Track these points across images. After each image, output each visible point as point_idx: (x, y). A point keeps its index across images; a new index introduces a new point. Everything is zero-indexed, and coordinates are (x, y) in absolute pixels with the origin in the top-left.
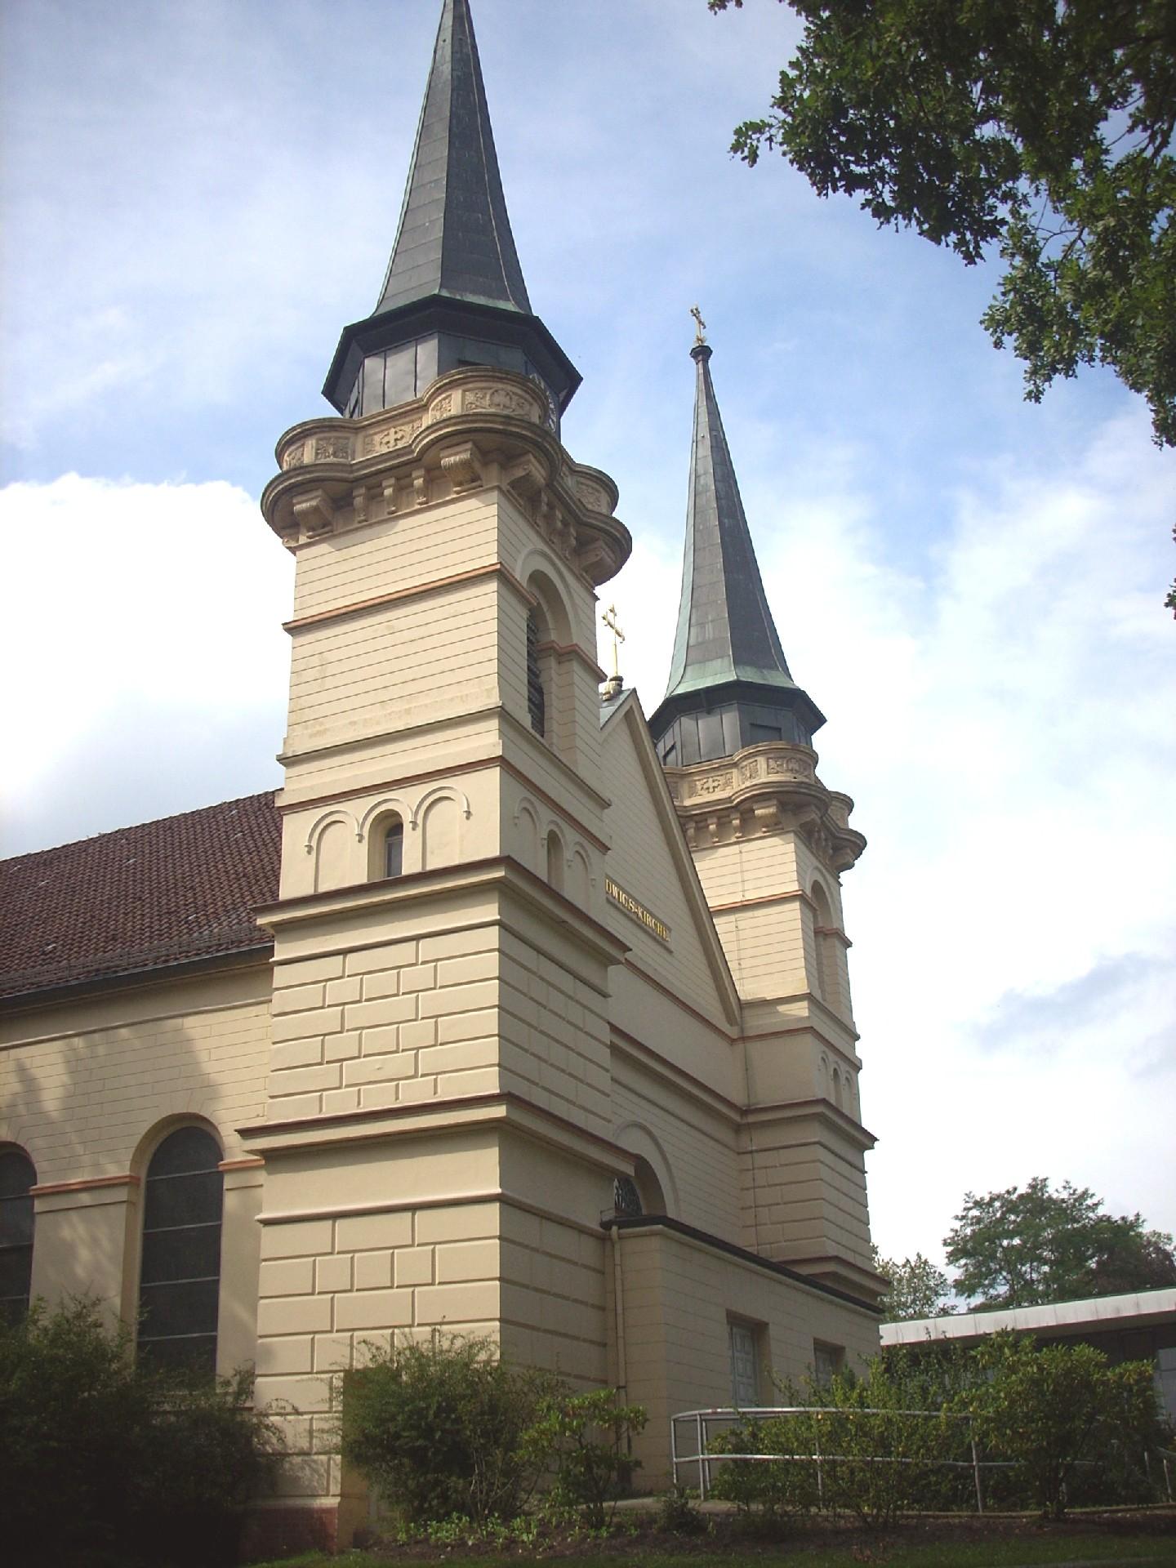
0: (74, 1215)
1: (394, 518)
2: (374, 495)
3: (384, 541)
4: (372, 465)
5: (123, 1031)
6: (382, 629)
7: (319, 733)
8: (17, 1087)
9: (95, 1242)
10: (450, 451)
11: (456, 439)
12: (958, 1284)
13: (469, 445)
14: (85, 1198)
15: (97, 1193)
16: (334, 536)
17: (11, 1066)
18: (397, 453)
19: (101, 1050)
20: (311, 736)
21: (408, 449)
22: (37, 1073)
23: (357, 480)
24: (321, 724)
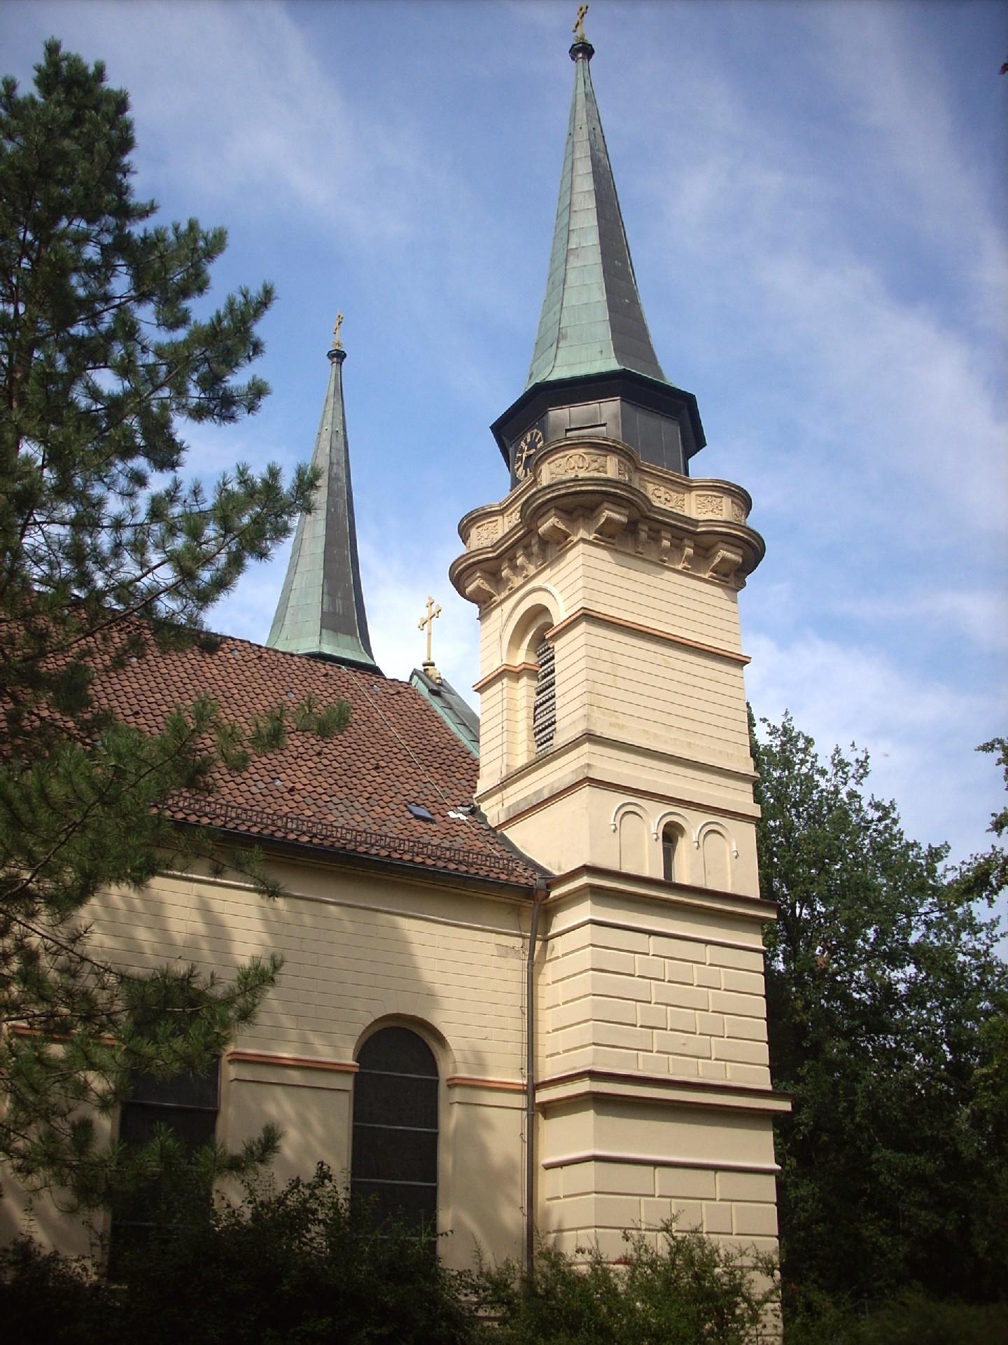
0: (278, 1091)
1: (661, 565)
2: (655, 538)
3: (562, 565)
4: (662, 515)
5: (332, 908)
6: (660, 659)
7: (622, 727)
8: (200, 927)
9: (305, 1125)
10: (732, 548)
11: (738, 542)
12: (101, 1097)
13: (553, 512)
14: (296, 1076)
15: (308, 1073)
16: (616, 550)
17: (193, 902)
18: (688, 520)
19: (307, 920)
20: (612, 725)
21: (696, 522)
22: (228, 920)
23: (647, 518)
24: (617, 718)
